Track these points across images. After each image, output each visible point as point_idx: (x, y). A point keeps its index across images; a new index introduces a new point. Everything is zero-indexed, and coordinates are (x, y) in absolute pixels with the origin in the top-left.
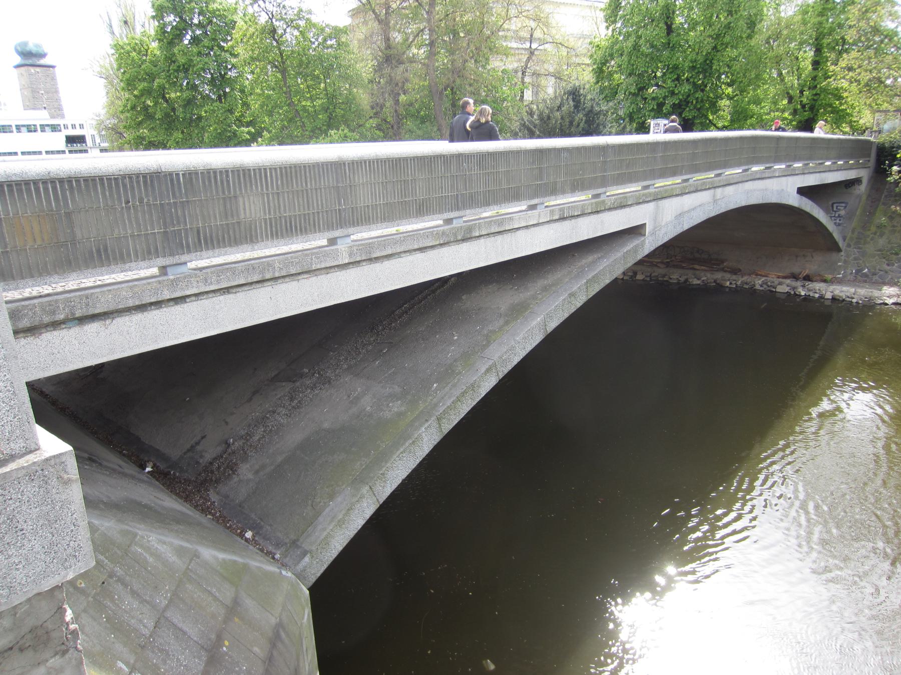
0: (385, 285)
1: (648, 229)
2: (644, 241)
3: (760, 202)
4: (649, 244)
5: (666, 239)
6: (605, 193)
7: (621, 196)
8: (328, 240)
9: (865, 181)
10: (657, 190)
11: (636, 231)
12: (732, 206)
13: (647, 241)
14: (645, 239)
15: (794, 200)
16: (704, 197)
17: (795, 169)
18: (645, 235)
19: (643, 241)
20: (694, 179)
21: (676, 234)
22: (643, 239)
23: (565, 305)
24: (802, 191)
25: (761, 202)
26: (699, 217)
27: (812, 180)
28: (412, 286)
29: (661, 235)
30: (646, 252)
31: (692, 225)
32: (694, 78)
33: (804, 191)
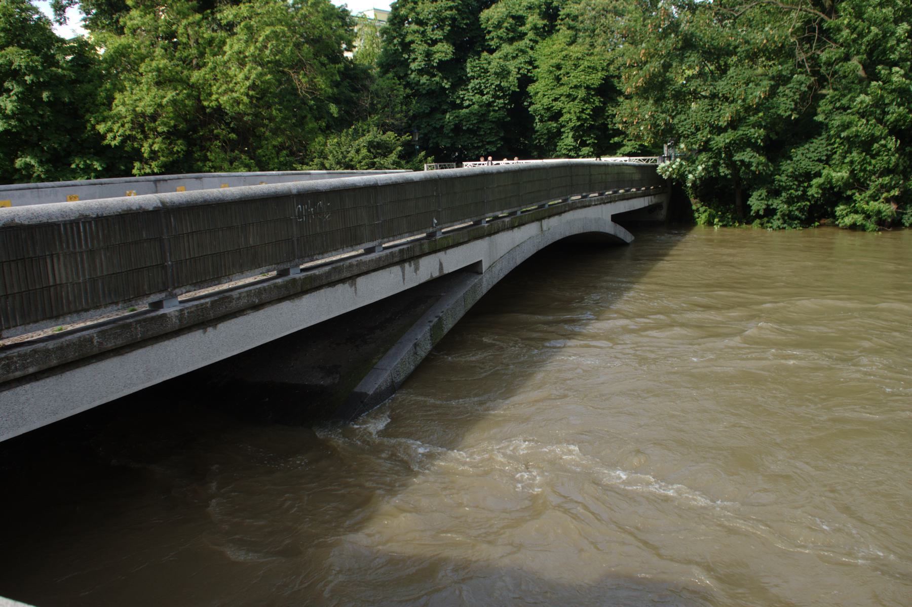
0: (221, 351)
1: (485, 266)
2: (481, 279)
3: (582, 232)
4: (487, 281)
5: (502, 276)
6: (380, 245)
7: (28, 349)
8: (365, 250)
9: (665, 205)
10: (388, 251)
11: (474, 269)
12: (558, 237)
13: (484, 280)
14: (482, 278)
15: (610, 228)
16: (531, 230)
17: (574, 202)
18: (482, 273)
19: (481, 279)
20: (443, 231)
21: (511, 270)
22: (480, 277)
23: (411, 357)
24: (616, 218)
25: (581, 231)
26: (529, 251)
27: (622, 207)
28: (249, 350)
29: (497, 272)
30: (485, 291)
31: (524, 259)
32: (204, 92)
33: (617, 219)
